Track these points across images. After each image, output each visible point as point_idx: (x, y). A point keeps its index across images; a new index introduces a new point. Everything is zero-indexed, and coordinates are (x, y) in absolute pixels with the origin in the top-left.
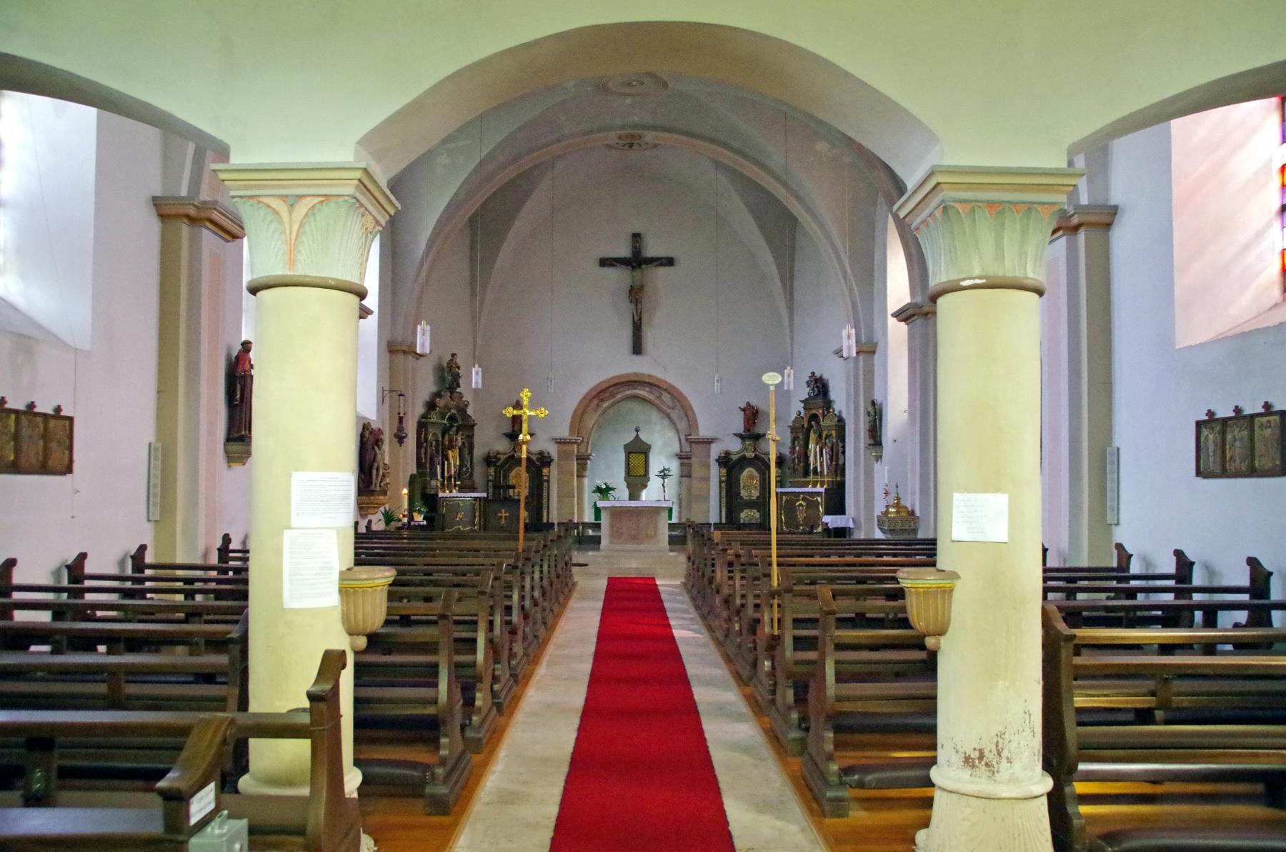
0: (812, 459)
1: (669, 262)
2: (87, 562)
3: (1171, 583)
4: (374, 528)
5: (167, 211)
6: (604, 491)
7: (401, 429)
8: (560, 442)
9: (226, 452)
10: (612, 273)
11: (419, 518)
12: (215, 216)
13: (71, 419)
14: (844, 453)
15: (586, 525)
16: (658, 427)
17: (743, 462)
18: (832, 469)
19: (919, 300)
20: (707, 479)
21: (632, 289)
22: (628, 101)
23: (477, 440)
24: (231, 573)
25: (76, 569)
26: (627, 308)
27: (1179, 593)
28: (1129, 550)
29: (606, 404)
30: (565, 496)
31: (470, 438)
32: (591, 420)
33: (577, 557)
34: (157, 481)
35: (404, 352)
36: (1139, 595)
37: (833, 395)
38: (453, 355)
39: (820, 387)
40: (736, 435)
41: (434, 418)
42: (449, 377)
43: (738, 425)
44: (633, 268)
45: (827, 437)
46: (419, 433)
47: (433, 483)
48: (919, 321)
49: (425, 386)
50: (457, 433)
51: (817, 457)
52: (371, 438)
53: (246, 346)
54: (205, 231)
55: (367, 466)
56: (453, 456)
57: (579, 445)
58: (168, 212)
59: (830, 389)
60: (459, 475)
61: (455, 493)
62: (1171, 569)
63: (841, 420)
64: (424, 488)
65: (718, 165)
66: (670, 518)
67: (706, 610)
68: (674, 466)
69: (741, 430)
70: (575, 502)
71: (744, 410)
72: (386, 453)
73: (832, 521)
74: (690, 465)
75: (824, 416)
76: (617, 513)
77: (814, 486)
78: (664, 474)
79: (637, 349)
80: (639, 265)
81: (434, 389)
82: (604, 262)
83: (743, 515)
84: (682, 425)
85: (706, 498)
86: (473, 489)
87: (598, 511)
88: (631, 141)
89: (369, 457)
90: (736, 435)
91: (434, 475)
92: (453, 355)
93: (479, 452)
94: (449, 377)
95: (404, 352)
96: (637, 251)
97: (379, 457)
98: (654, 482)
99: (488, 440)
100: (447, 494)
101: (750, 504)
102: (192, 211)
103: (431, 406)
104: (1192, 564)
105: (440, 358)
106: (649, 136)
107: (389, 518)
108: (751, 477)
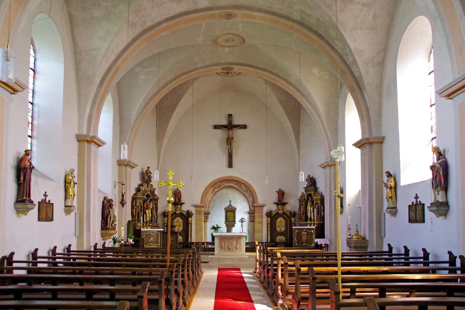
0: (309, 214)
1: (245, 127)
2: (14, 256)
3: (403, 256)
4: (107, 246)
5: (80, 139)
6: (216, 228)
7: (123, 200)
8: (196, 206)
9: (16, 208)
10: (219, 131)
11: (131, 241)
12: (131, 164)
13: (53, 204)
14: (324, 211)
15: (208, 243)
16: (239, 201)
17: (278, 215)
18: (319, 217)
19: (367, 136)
20: (261, 223)
21: (228, 139)
22: (227, 50)
23: (159, 206)
24: (72, 260)
25: (34, 254)
26: (225, 146)
27: (405, 259)
28: (409, 248)
29: (216, 190)
30: (199, 230)
31: (156, 205)
32: (209, 196)
33: (203, 257)
34: (78, 224)
35: (125, 165)
36: (411, 264)
37: (318, 185)
38: (148, 168)
39: (312, 182)
40: (275, 203)
41: (139, 195)
42: (146, 177)
43: (275, 198)
44: (229, 129)
45: (316, 203)
46: (132, 202)
47: (139, 224)
48: (367, 147)
49: (135, 181)
50: (150, 202)
51: (311, 212)
52: (108, 204)
53: (27, 153)
54: (92, 145)
55: (105, 217)
56: (148, 212)
57: (205, 208)
58: (81, 139)
59: (317, 182)
60: (151, 221)
61: (149, 229)
62: (447, 259)
63: (322, 196)
64: (135, 227)
65: (267, 82)
66: (246, 240)
67: (271, 292)
68: (246, 217)
69: (277, 201)
70: (201, 233)
71: (278, 192)
72: (116, 211)
73: (319, 241)
74: (254, 217)
75: (314, 194)
76: (222, 238)
77: (310, 226)
78: (242, 221)
79: (230, 165)
80: (232, 128)
81: (140, 182)
82: (216, 127)
83: (277, 238)
84: (250, 199)
85: (261, 231)
86: (157, 227)
87: (213, 237)
88: (228, 71)
89: (106, 212)
90: (275, 203)
91: (139, 221)
92: (148, 168)
93: (160, 211)
94: (146, 177)
95: (125, 165)
96: (230, 122)
97: (111, 212)
98: (238, 224)
99: (165, 204)
100: (145, 229)
101: (281, 234)
102: (88, 139)
103: (138, 190)
104: (409, 250)
105: (142, 169)
106: (236, 69)
107: (115, 241)
108: (281, 222)
